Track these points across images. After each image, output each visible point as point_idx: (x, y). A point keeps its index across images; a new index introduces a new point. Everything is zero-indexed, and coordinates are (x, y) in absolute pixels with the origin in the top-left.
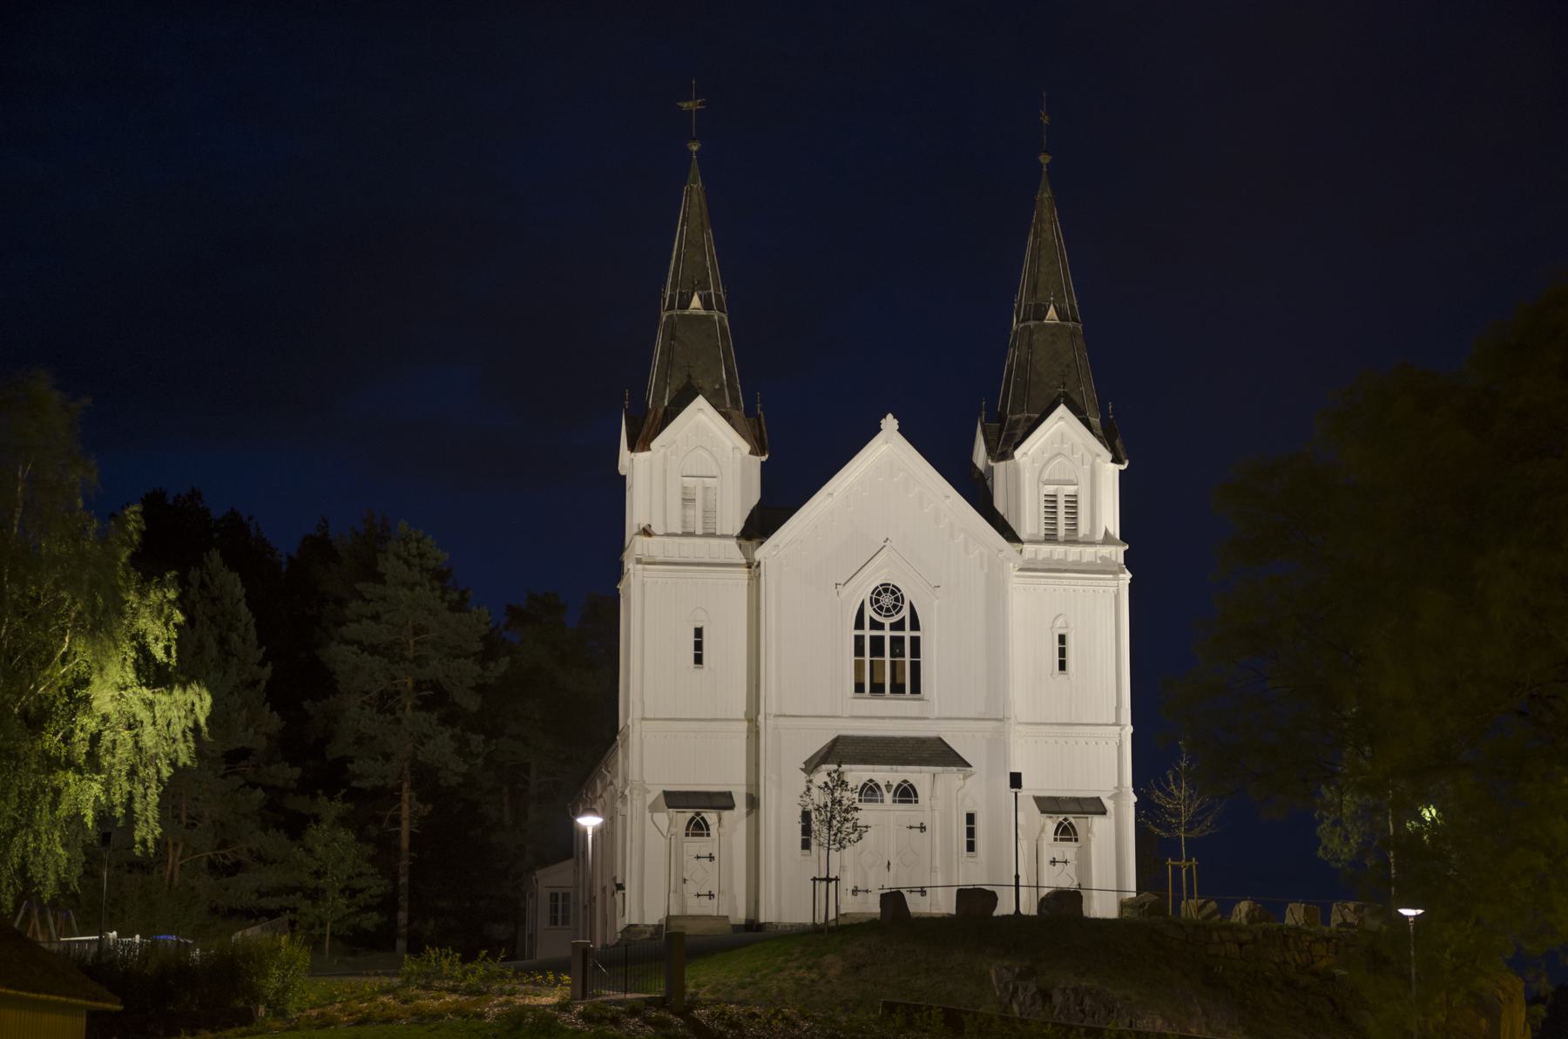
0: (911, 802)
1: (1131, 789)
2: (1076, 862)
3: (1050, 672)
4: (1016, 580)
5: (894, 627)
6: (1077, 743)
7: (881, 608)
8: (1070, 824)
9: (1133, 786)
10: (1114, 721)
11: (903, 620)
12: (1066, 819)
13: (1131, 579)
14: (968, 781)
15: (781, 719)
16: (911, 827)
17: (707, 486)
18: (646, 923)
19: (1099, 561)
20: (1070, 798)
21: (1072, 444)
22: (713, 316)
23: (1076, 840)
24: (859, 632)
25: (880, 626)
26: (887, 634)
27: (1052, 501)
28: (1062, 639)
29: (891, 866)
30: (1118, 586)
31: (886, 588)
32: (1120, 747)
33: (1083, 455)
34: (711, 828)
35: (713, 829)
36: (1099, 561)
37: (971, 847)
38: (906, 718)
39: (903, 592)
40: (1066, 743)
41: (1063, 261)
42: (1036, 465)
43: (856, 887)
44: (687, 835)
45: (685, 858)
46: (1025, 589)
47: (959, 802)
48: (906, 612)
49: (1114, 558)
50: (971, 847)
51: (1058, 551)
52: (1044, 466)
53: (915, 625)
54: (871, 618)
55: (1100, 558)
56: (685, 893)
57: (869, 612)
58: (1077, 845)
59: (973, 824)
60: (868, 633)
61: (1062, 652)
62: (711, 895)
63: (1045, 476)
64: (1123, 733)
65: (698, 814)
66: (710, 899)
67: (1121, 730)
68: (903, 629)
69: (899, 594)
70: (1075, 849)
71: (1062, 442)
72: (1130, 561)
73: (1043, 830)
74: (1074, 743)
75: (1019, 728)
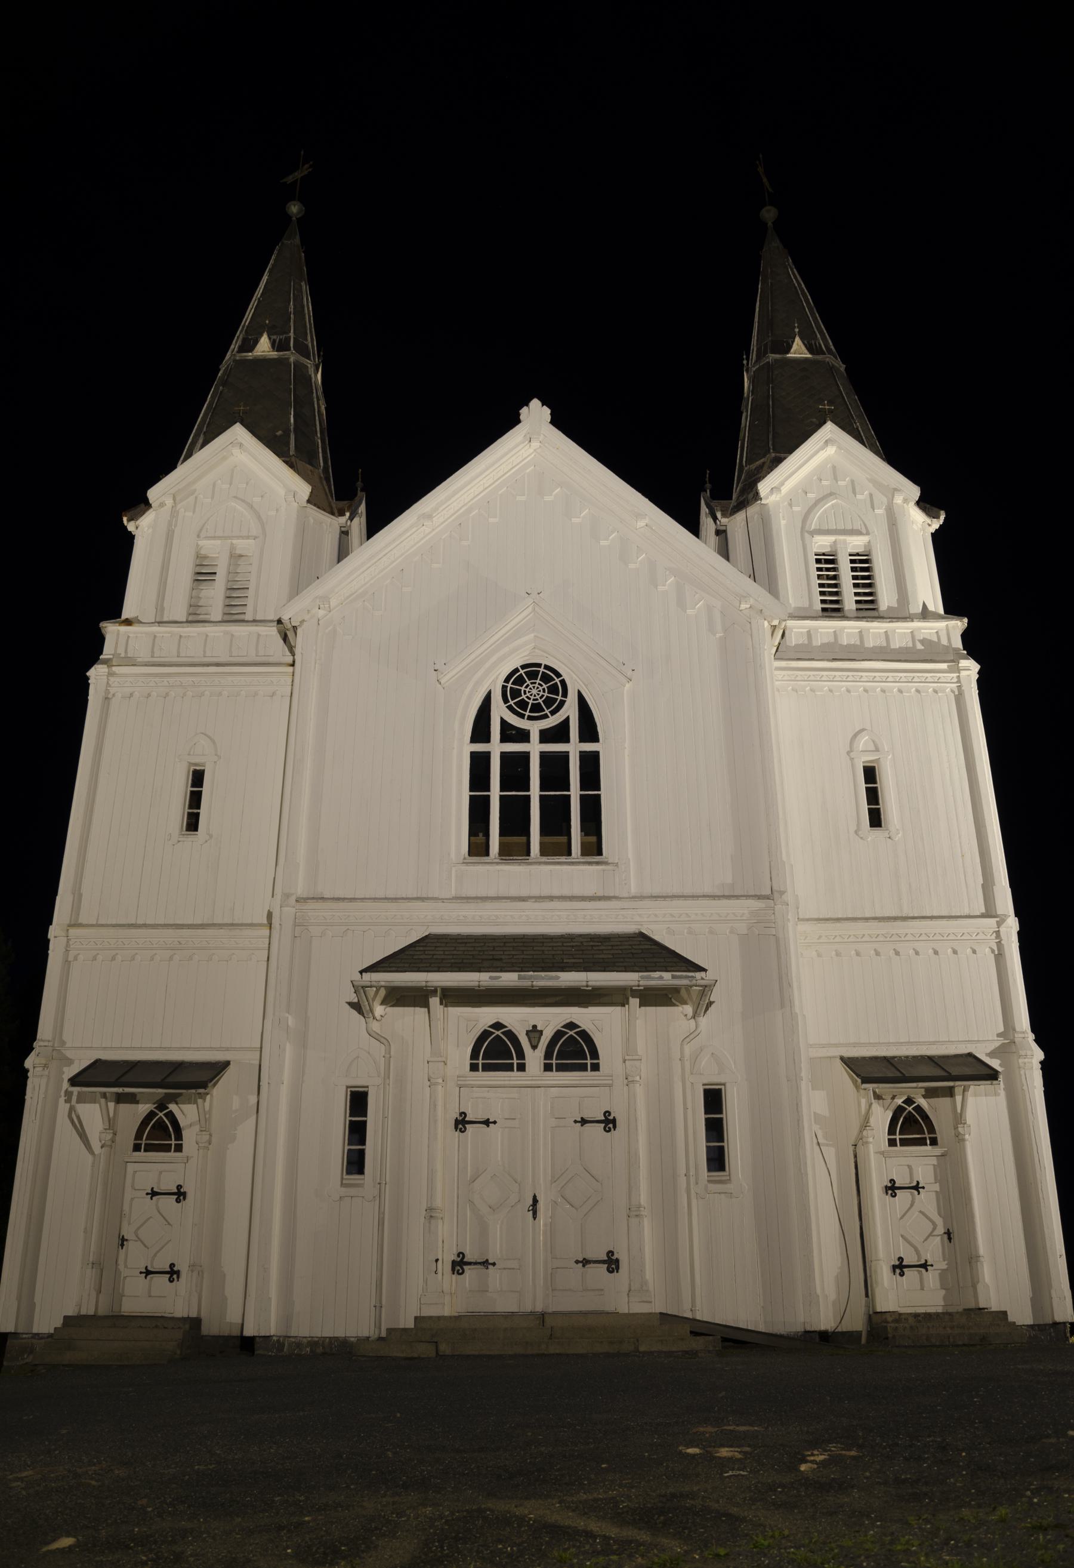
0: (583, 1068)
1: (1031, 1037)
2: (937, 1187)
3: (853, 828)
4: (780, 674)
5: (546, 736)
6: (917, 953)
7: (523, 705)
8: (919, 1109)
9: (1034, 1029)
10: (983, 911)
11: (566, 722)
12: (909, 1101)
13: (979, 673)
14: (703, 1021)
15: (312, 905)
16: (584, 1122)
17: (238, 552)
18: (35, 1331)
19: (919, 646)
20: (914, 1057)
21: (852, 482)
22: (288, 359)
23: (934, 1142)
24: (480, 747)
25: (523, 736)
26: (535, 748)
27: (827, 562)
28: (870, 774)
29: (541, 1206)
30: (959, 681)
31: (531, 671)
32: (1000, 957)
33: (871, 495)
34: (185, 1134)
35: (189, 1137)
36: (919, 646)
37: (717, 1160)
38: (572, 898)
39: (565, 676)
40: (897, 953)
41: (821, 332)
42: (795, 509)
43: (461, 1254)
44: (137, 1148)
45: (128, 1194)
46: (795, 690)
47: (687, 1064)
48: (570, 710)
49: (944, 641)
50: (717, 1160)
51: (848, 629)
52: (818, 502)
53: (589, 731)
54: (503, 722)
55: (920, 641)
56: (121, 1267)
57: (499, 711)
58: (937, 1151)
59: (721, 1112)
60: (496, 748)
61: (873, 796)
62: (173, 1273)
63: (814, 524)
64: (1002, 929)
65: (162, 1106)
66: (171, 1281)
67: (999, 924)
68: (566, 739)
69: (557, 680)
70: (934, 1161)
71: (836, 479)
72: (972, 644)
73: (865, 1124)
74: (911, 952)
75: (802, 927)
